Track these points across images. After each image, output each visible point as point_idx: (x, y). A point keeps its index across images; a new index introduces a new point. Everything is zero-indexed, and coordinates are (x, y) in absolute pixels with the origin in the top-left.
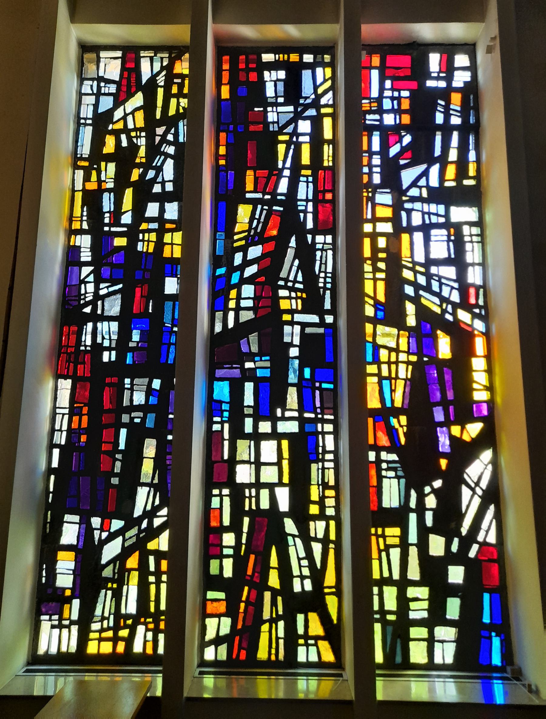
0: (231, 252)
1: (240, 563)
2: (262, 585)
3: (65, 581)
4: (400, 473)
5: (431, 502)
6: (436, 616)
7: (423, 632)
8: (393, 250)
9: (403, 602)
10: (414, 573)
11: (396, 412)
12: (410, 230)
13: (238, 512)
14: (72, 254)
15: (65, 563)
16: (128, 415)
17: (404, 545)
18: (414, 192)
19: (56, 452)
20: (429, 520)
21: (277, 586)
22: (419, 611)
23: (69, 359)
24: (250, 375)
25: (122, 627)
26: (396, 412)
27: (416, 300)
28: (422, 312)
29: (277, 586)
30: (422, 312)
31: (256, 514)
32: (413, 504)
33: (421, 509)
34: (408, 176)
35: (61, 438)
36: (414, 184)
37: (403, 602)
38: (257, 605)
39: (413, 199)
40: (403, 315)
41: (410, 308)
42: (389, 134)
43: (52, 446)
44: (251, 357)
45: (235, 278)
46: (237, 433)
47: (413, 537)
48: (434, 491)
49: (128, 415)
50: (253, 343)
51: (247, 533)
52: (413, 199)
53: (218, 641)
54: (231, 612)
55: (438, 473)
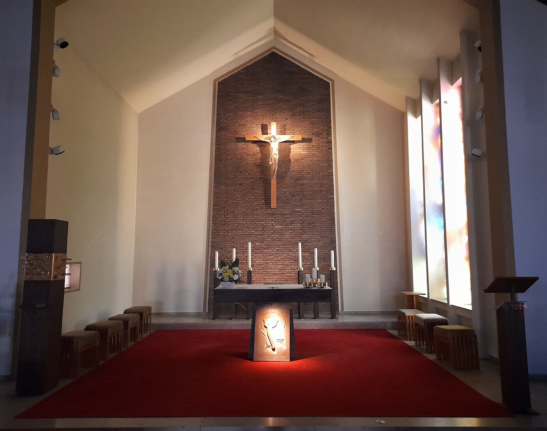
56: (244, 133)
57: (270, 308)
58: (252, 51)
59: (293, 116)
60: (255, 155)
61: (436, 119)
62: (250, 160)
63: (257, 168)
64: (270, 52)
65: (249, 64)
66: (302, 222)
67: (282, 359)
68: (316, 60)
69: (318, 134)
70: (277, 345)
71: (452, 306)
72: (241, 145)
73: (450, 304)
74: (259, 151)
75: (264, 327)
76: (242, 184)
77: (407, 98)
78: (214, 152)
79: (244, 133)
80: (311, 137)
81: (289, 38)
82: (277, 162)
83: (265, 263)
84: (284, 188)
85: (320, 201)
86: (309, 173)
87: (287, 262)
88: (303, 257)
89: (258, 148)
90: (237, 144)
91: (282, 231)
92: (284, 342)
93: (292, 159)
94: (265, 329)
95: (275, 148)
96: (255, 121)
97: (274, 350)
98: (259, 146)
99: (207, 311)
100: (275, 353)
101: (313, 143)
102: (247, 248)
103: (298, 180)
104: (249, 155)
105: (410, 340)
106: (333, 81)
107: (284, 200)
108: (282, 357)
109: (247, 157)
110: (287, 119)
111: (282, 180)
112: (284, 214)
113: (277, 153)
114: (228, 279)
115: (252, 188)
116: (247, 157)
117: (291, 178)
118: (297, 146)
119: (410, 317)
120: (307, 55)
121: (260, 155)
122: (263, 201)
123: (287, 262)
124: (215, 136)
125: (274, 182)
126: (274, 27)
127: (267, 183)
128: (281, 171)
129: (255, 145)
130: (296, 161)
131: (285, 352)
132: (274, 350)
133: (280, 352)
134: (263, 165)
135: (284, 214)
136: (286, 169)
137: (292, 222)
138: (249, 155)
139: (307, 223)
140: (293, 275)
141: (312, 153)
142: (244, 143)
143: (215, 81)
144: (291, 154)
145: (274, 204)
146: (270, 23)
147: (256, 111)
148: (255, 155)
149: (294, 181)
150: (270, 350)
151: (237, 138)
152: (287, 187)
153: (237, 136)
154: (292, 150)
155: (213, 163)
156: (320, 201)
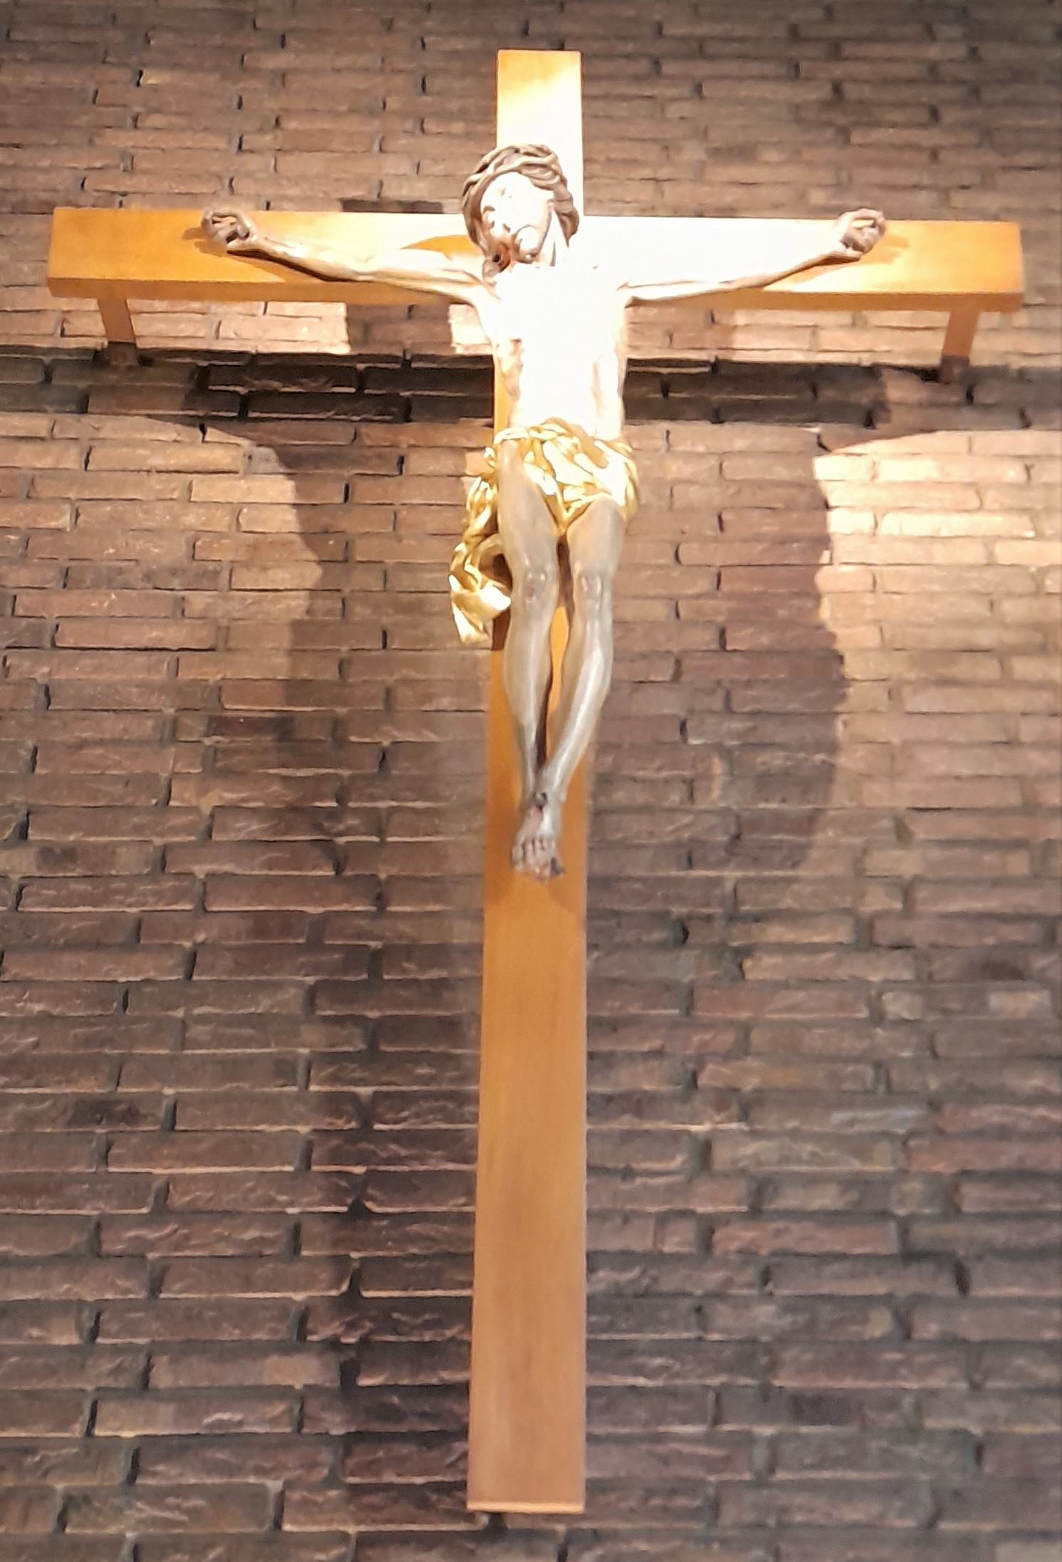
59: (841, 114)
62: (118, 651)
63: (218, 768)
74: (287, 521)
84: (747, 1107)
88: (139, 1083)
89: (282, 489)
95: (559, 423)
98: (292, 463)
104: (112, 579)
107: (752, 1353)
109: (60, 604)
111: (685, 967)
115: (98, 1110)
116: (60, 604)
117: (867, 938)
118: (924, 469)
121: (295, 577)
122: (304, 1371)
125: (532, 969)
127: (395, 1014)
128: (683, 827)
134: (342, 757)
136: (765, 782)
138: (112, 579)
144: (833, 577)
147: (281, 60)
149: (925, 984)
152: (801, 1100)
154: (837, 523)
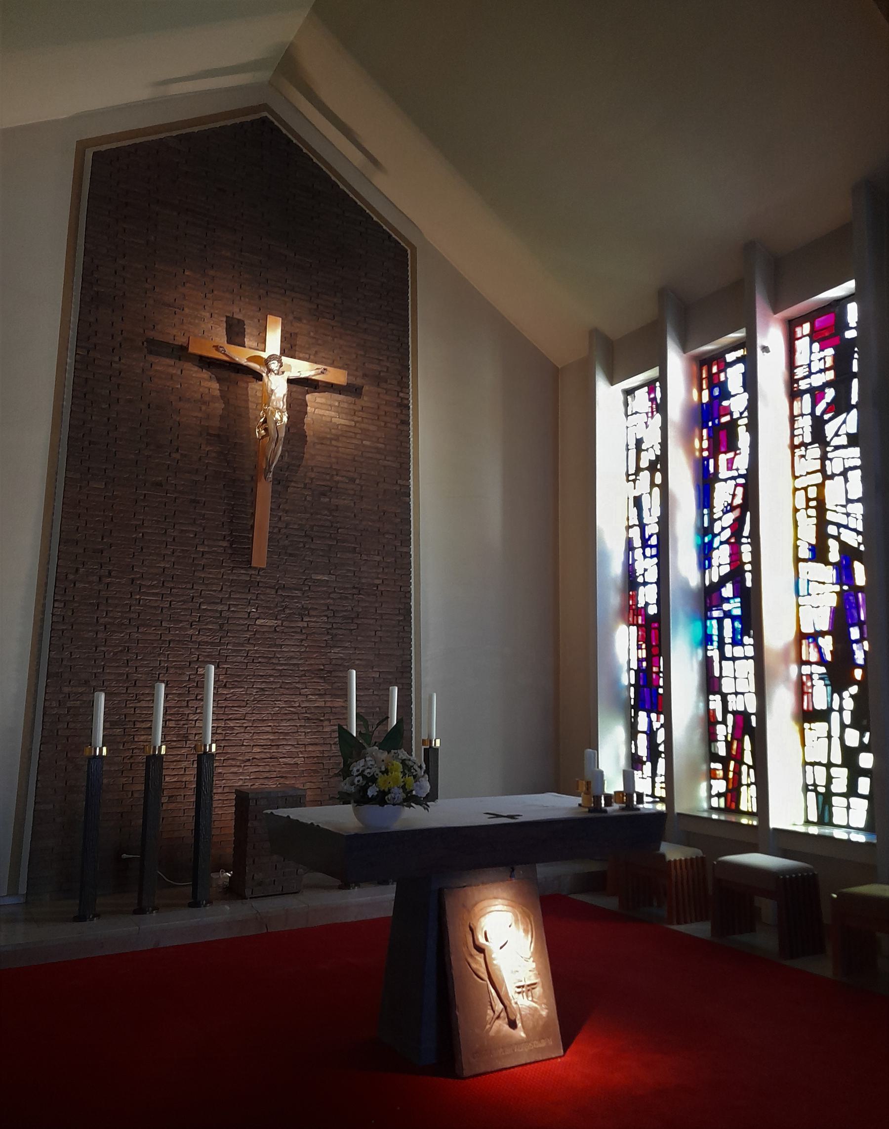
0: (712, 521)
1: (729, 745)
2: (740, 762)
3: (643, 752)
4: (828, 682)
5: (849, 704)
6: (852, 791)
7: (843, 801)
8: (821, 498)
9: (830, 779)
10: (837, 758)
11: (822, 634)
12: (832, 477)
13: (725, 711)
14: (629, 541)
15: (642, 740)
16: (825, 627)
17: (829, 737)
18: (836, 442)
19: (632, 673)
20: (847, 720)
21: (751, 763)
22: (840, 784)
23: (632, 612)
24: (728, 614)
25: (862, 592)
26: (822, 634)
27: (837, 538)
28: (844, 547)
29: (751, 763)
30: (844, 547)
31: (735, 713)
32: (836, 706)
33: (841, 710)
34: (830, 429)
35: (634, 665)
36: (837, 435)
37: (830, 779)
38: (738, 773)
39: (837, 448)
40: (827, 550)
41: (833, 545)
42: (817, 394)
43: (630, 669)
44: (727, 600)
45: (716, 543)
46: (723, 657)
47: (836, 732)
48: (851, 696)
49: (825, 627)
50: (727, 591)
51: (717, 741)
52: (837, 448)
53: (719, 795)
54: (725, 777)
55: (854, 682)
56: (174, 332)
57: (494, 882)
58: (228, 90)
60: (204, 403)
61: (689, 392)
64: (257, 116)
65: (196, 129)
66: (330, 614)
67: (539, 1050)
68: (380, 180)
69: (377, 379)
70: (522, 1003)
71: (775, 830)
72: (164, 365)
73: (773, 824)
74: (217, 393)
75: (474, 952)
76: (159, 484)
77: (595, 334)
78: (70, 368)
79: (174, 332)
80: (359, 382)
81: (325, 94)
82: (282, 434)
83: (224, 728)
85: (378, 558)
86: (353, 480)
87: (285, 726)
89: (215, 386)
90: (151, 358)
91: (275, 636)
92: (538, 991)
93: (309, 433)
94: (480, 958)
96: (209, 302)
97: (513, 1024)
98: (219, 380)
99: (23, 890)
100: (520, 1033)
101: (365, 401)
102: (201, 685)
103: (324, 494)
105: (686, 922)
106: (414, 249)
108: (543, 1044)
110: (300, 319)
112: (284, 587)
113: (282, 405)
114: (400, 795)
118: (323, 400)
119: (683, 863)
120: (356, 157)
121: (219, 406)
122: (225, 544)
123: (285, 726)
124: (74, 319)
126: (292, 44)
129: (205, 374)
130: (322, 440)
131: (546, 1026)
132: (513, 1024)
133: (534, 1027)
135: (284, 587)
137: (304, 612)
139: (344, 618)
140: (299, 761)
141: (363, 426)
142: (172, 362)
143: (82, 146)
144: (307, 420)
145: (260, 556)
146: (285, 27)
147: (212, 273)
148: (204, 403)
150: (502, 1025)
151: (151, 342)
153: (151, 334)
155: (67, 404)
156: (378, 558)
